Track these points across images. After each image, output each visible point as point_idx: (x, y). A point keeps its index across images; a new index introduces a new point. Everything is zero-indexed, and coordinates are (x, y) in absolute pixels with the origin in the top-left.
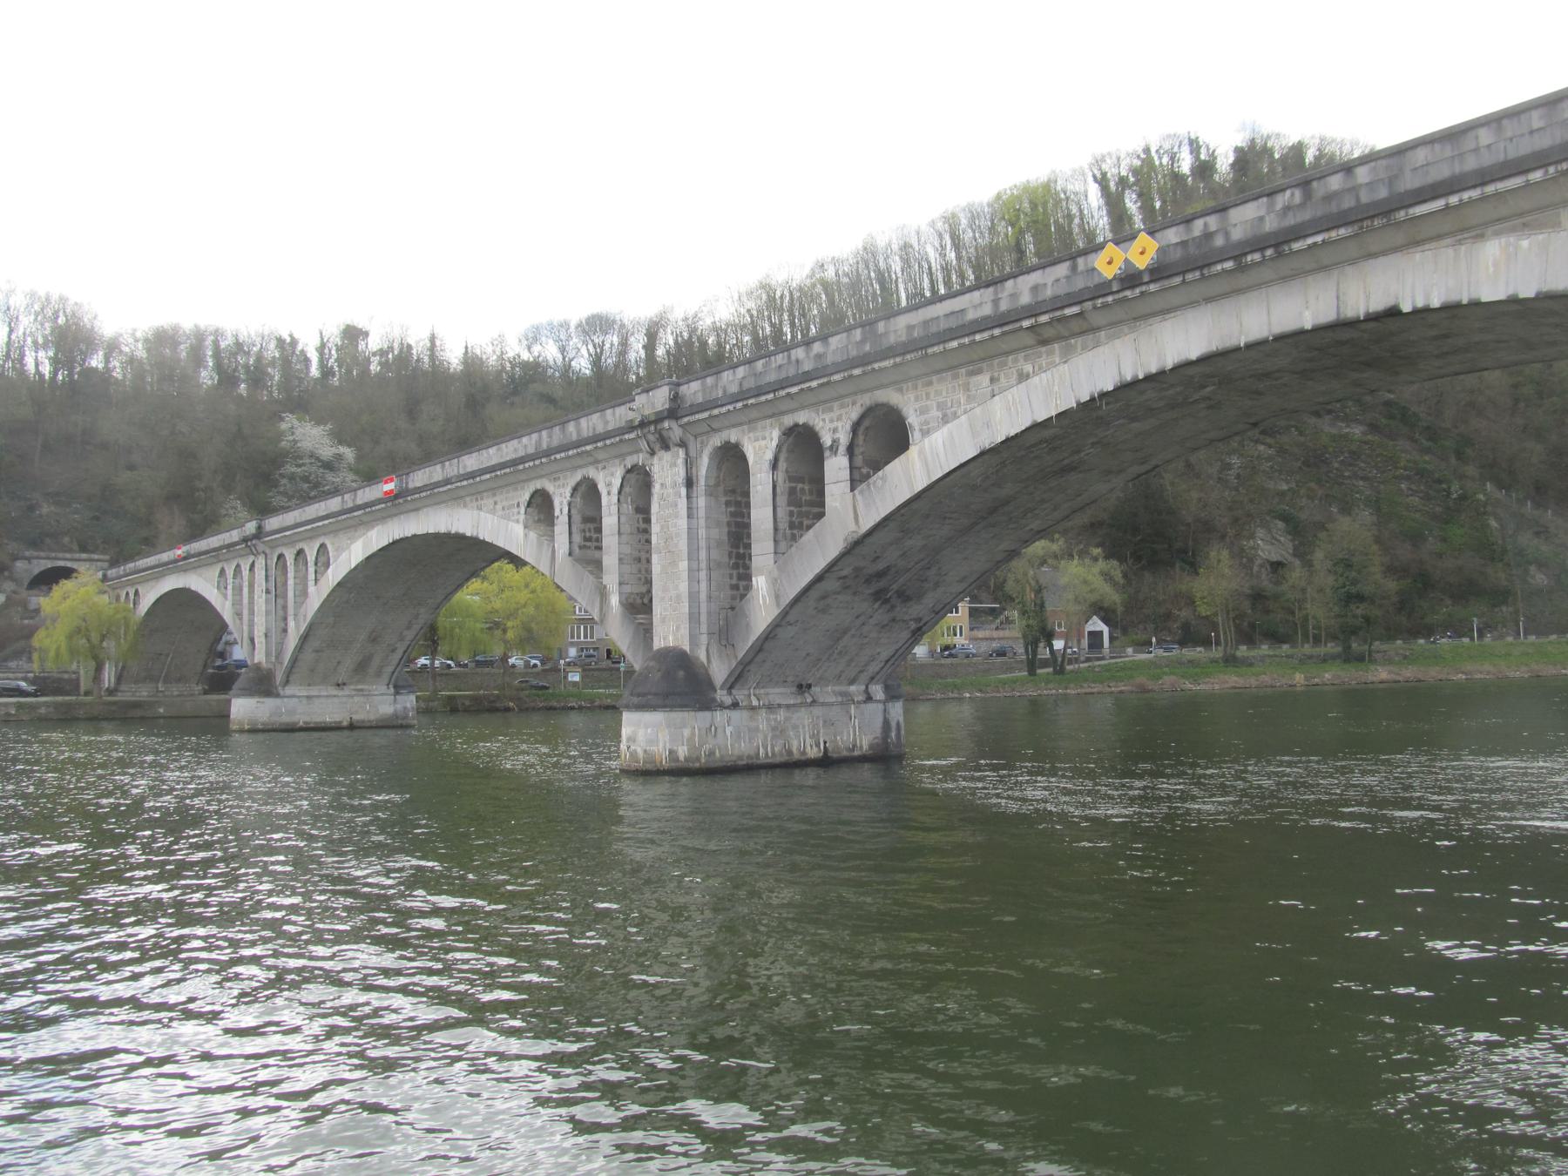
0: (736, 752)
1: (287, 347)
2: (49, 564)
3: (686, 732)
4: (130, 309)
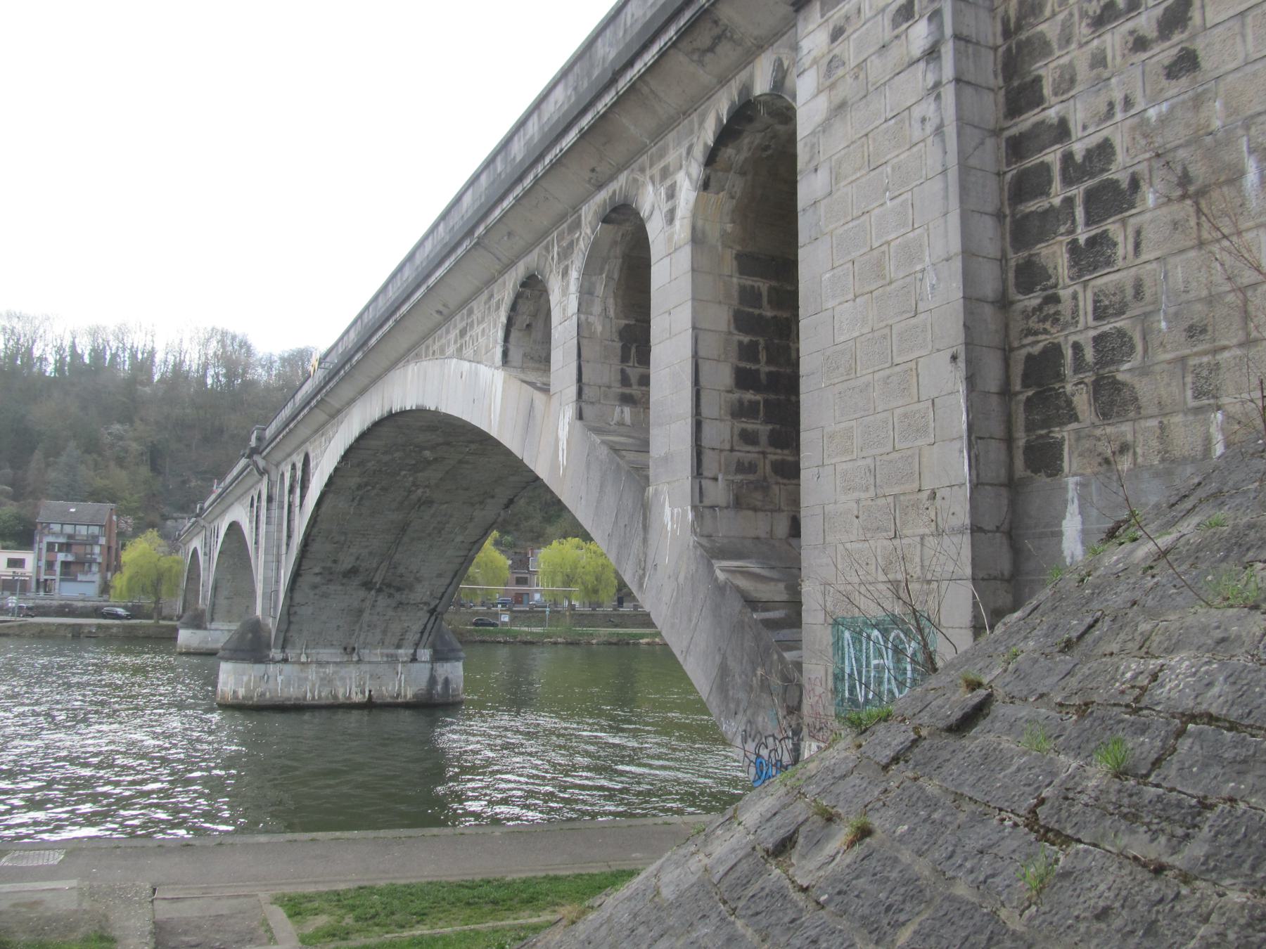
0: (285, 695)
3: (245, 678)
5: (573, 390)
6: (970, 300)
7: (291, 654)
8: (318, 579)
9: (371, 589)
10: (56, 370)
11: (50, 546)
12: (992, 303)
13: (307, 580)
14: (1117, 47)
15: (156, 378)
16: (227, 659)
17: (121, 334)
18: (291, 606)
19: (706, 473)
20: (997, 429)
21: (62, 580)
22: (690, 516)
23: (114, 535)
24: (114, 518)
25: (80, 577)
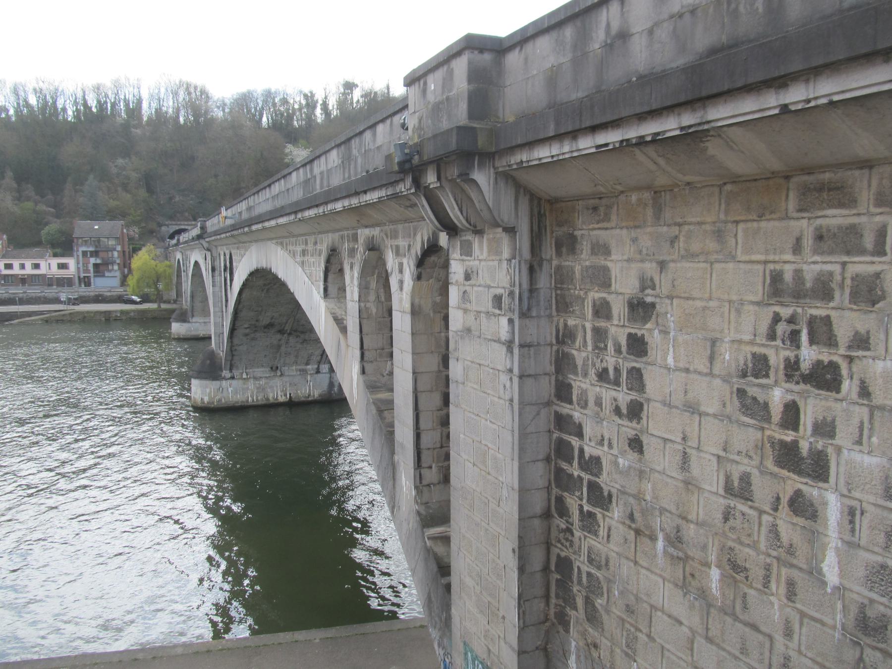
0: (235, 399)
1: (310, 102)
2: (177, 228)
3: (208, 390)
4: (223, 87)
5: (358, 353)
6: (524, 520)
7: (236, 373)
8: (247, 331)
9: (284, 334)
10: (74, 117)
11: (85, 253)
12: (540, 516)
13: (240, 332)
14: (608, 399)
15: (145, 119)
16: (195, 378)
17: (117, 85)
18: (232, 346)
19: (424, 465)
20: (539, 591)
21: (95, 276)
22: (414, 493)
23: (126, 243)
24: (125, 231)
25: (107, 274)
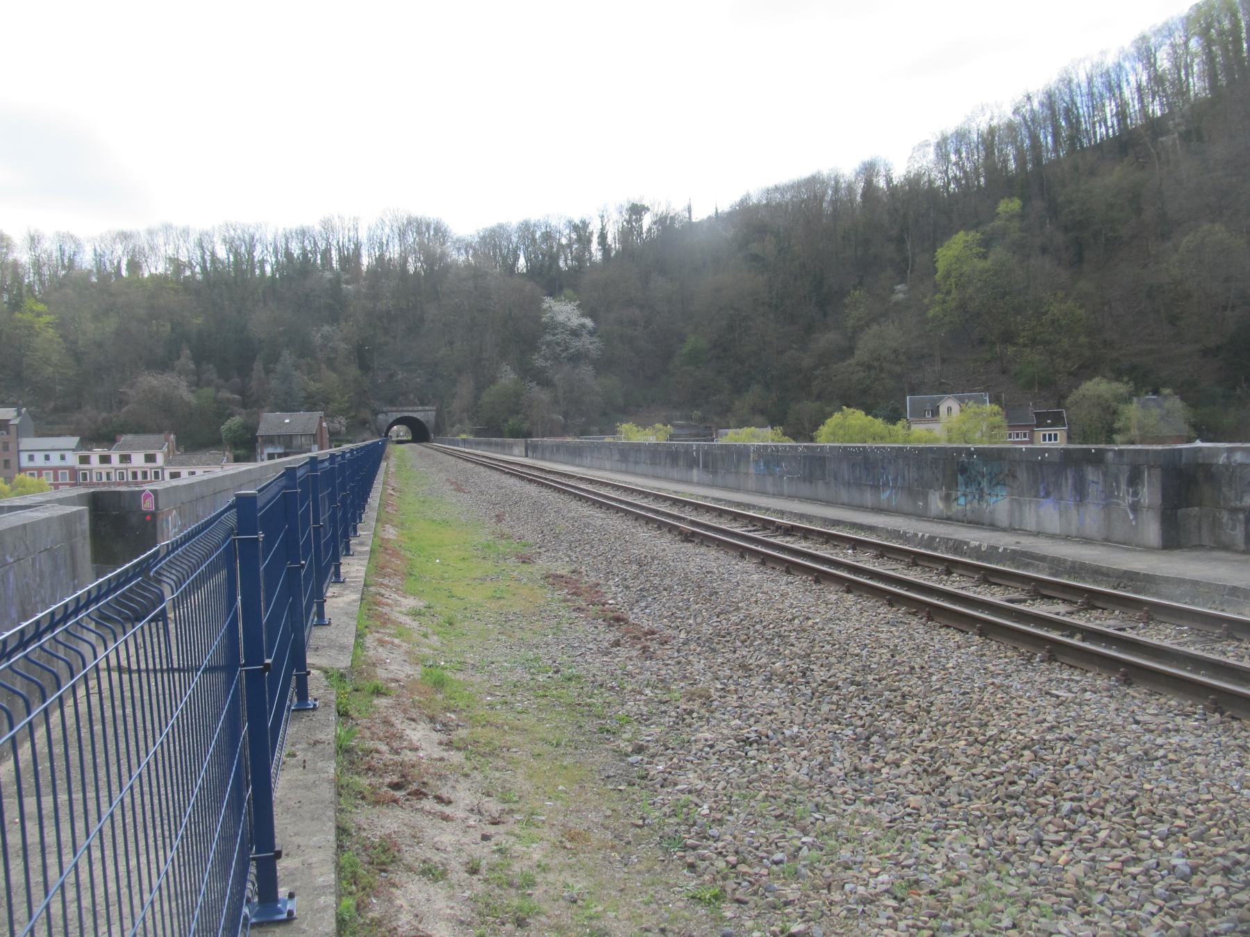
17: (327, 226)
